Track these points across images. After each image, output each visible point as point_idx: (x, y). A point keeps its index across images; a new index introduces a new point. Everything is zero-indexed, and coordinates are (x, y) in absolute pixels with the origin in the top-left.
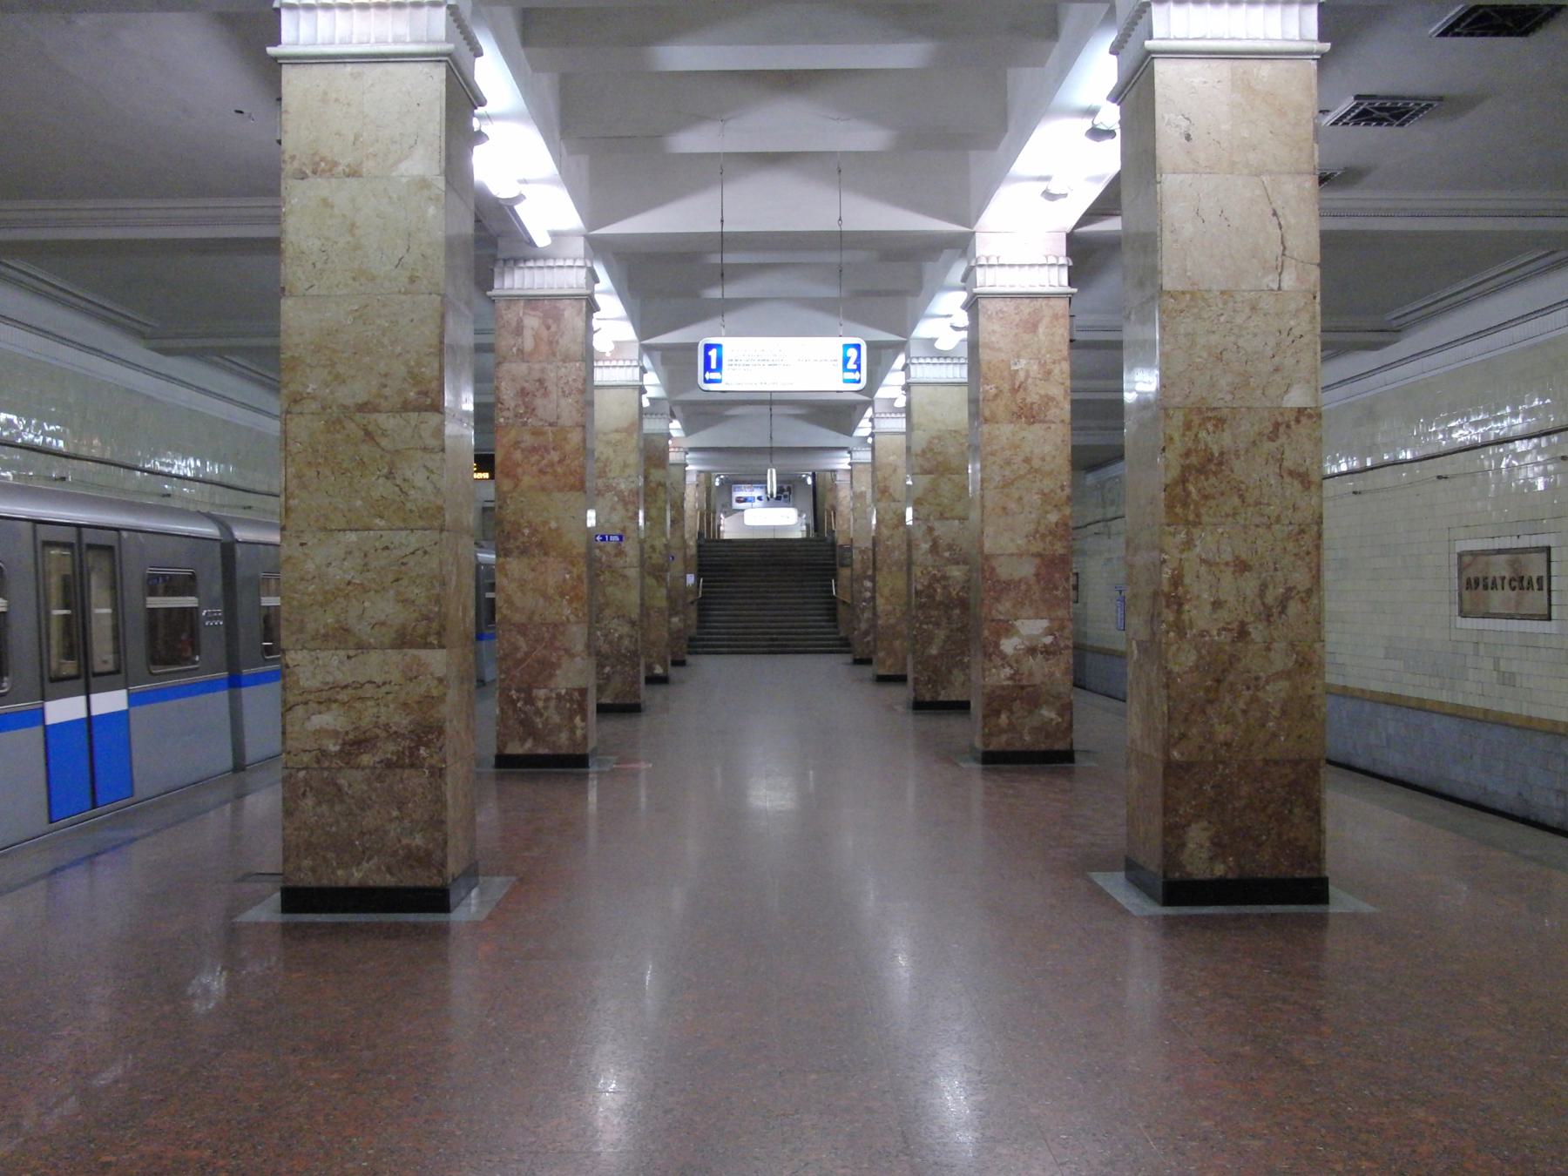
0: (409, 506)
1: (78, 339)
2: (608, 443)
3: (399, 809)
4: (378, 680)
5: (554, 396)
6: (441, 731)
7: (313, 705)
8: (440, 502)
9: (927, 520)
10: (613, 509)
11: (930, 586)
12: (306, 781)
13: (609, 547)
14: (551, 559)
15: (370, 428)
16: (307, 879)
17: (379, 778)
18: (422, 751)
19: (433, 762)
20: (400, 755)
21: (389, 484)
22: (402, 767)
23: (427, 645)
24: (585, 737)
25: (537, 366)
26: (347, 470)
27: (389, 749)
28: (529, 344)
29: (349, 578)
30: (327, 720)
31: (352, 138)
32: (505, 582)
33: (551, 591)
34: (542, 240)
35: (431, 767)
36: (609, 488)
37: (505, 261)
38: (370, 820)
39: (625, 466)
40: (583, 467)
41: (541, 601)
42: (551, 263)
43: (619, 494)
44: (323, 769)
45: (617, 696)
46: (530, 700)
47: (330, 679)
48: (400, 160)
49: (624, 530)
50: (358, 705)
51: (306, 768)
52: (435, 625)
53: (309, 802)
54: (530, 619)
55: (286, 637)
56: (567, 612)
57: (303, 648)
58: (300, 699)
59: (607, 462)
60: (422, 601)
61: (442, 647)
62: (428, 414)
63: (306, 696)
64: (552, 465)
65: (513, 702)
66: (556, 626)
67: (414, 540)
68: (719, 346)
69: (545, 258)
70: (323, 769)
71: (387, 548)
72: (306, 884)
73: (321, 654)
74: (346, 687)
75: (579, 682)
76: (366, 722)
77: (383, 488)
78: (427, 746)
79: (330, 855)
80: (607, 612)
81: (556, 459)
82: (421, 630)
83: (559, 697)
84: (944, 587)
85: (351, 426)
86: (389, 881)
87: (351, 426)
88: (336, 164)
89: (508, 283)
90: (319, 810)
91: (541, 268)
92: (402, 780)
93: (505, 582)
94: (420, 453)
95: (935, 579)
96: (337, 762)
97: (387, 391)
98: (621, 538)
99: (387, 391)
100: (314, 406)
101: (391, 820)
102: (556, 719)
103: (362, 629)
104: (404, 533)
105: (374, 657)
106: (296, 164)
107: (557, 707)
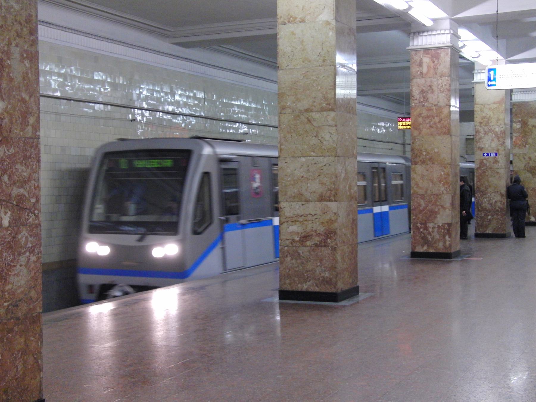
0: (323, 147)
1: (253, 74)
2: (490, 109)
3: (320, 262)
4: (313, 214)
5: (436, 93)
6: (335, 233)
7: (290, 223)
8: (335, 146)
10: (492, 140)
12: (288, 251)
13: (490, 159)
15: (309, 118)
16: (288, 288)
17: (313, 250)
18: (329, 241)
19: (333, 245)
20: (321, 242)
21: (316, 138)
22: (321, 246)
23: (330, 200)
24: (450, 245)
25: (429, 80)
26: (302, 134)
27: (317, 239)
28: (425, 69)
29: (302, 175)
30: (294, 228)
31: (301, 8)
32: (415, 176)
33: (435, 180)
34: (429, 24)
35: (332, 247)
36: (490, 130)
37: (414, 33)
38: (310, 266)
39: (499, 120)
40: (449, 124)
41: (431, 184)
42: (438, 32)
43: (496, 134)
44: (293, 246)
45: (494, 230)
46: (426, 228)
47: (296, 213)
48: (319, 15)
49: (498, 150)
50: (306, 222)
51: (288, 246)
52: (333, 193)
53: (289, 258)
54: (426, 192)
55: (281, 198)
56: (442, 189)
57: (287, 201)
58: (285, 220)
59: (489, 119)
60: (328, 183)
61: (335, 201)
62: (331, 112)
63: (288, 219)
64: (435, 123)
65: (419, 229)
66: (437, 195)
67: (326, 160)
68: (494, 70)
69: (432, 30)
70: (293, 246)
71: (316, 163)
72: (287, 289)
73: (293, 204)
74: (301, 216)
75: (448, 220)
76: (308, 230)
77: (314, 141)
78: (330, 239)
79: (296, 279)
80: (489, 190)
81: (437, 121)
82: (328, 194)
83: (439, 227)
85: (302, 117)
86: (317, 289)
87: (302, 117)
88: (296, 18)
89: (416, 43)
90: (292, 261)
91: (435, 35)
92: (321, 252)
93: (415, 176)
94: (328, 127)
96: (298, 244)
97: (315, 104)
98: (496, 154)
99: (315, 104)
100: (289, 111)
101: (317, 267)
102: (437, 237)
103: (307, 195)
104: (322, 158)
105: (311, 205)
106: (282, 19)
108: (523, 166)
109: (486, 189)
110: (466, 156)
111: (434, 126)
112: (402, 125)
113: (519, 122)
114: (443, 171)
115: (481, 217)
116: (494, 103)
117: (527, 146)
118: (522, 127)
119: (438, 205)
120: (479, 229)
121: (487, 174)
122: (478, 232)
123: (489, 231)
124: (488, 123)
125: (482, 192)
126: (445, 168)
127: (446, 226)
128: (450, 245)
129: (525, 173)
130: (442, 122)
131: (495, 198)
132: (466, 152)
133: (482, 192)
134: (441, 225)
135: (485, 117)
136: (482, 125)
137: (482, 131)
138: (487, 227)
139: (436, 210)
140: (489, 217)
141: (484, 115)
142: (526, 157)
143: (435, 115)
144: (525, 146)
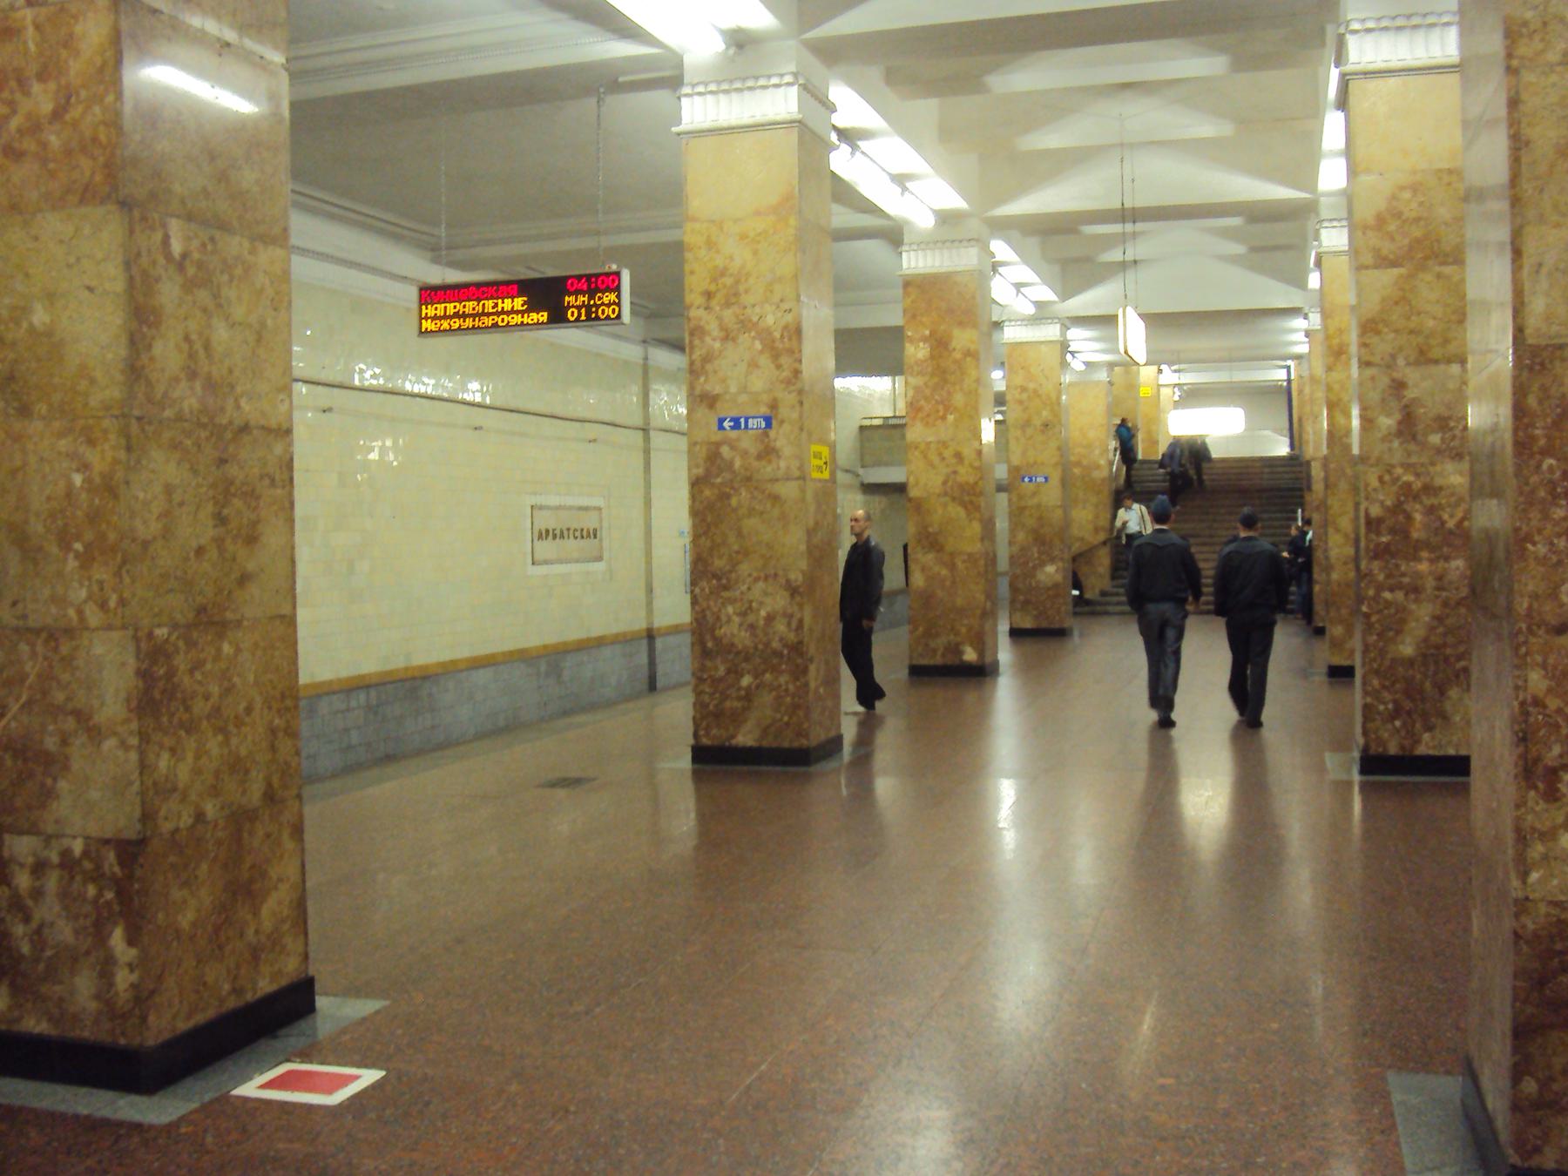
9: (1390, 365)
10: (753, 365)
11: (1397, 509)
14: (37, 426)
33: (37, 527)
36: (745, 325)
43: (765, 336)
45: (765, 731)
49: (774, 406)
64: (34, 127)
80: (745, 568)
81: (47, 107)
83: (68, 863)
84: (1431, 510)
95: (1407, 491)
98: (768, 420)
102: (64, 933)
107: (64, 895)
108: (939, 480)
109: (734, 565)
110: (861, 471)
111: (29, 145)
112: (435, 318)
113: (925, 339)
114: (84, 467)
115: (715, 682)
116: (758, 213)
117: (951, 418)
118: (932, 357)
119: (56, 711)
120: (707, 729)
121: (734, 502)
122: (705, 741)
123: (745, 738)
124: (736, 294)
125: (715, 576)
126: (91, 442)
127: (111, 856)
128: (142, 998)
129: (945, 505)
130: (75, 113)
131: (768, 600)
132: (862, 459)
133: (715, 576)
134: (78, 847)
135: (723, 272)
136: (714, 303)
137: (713, 327)
138: (737, 718)
139: (51, 743)
140: (746, 681)
141: (719, 262)
142: (948, 453)
143: (33, 68)
144: (944, 418)
